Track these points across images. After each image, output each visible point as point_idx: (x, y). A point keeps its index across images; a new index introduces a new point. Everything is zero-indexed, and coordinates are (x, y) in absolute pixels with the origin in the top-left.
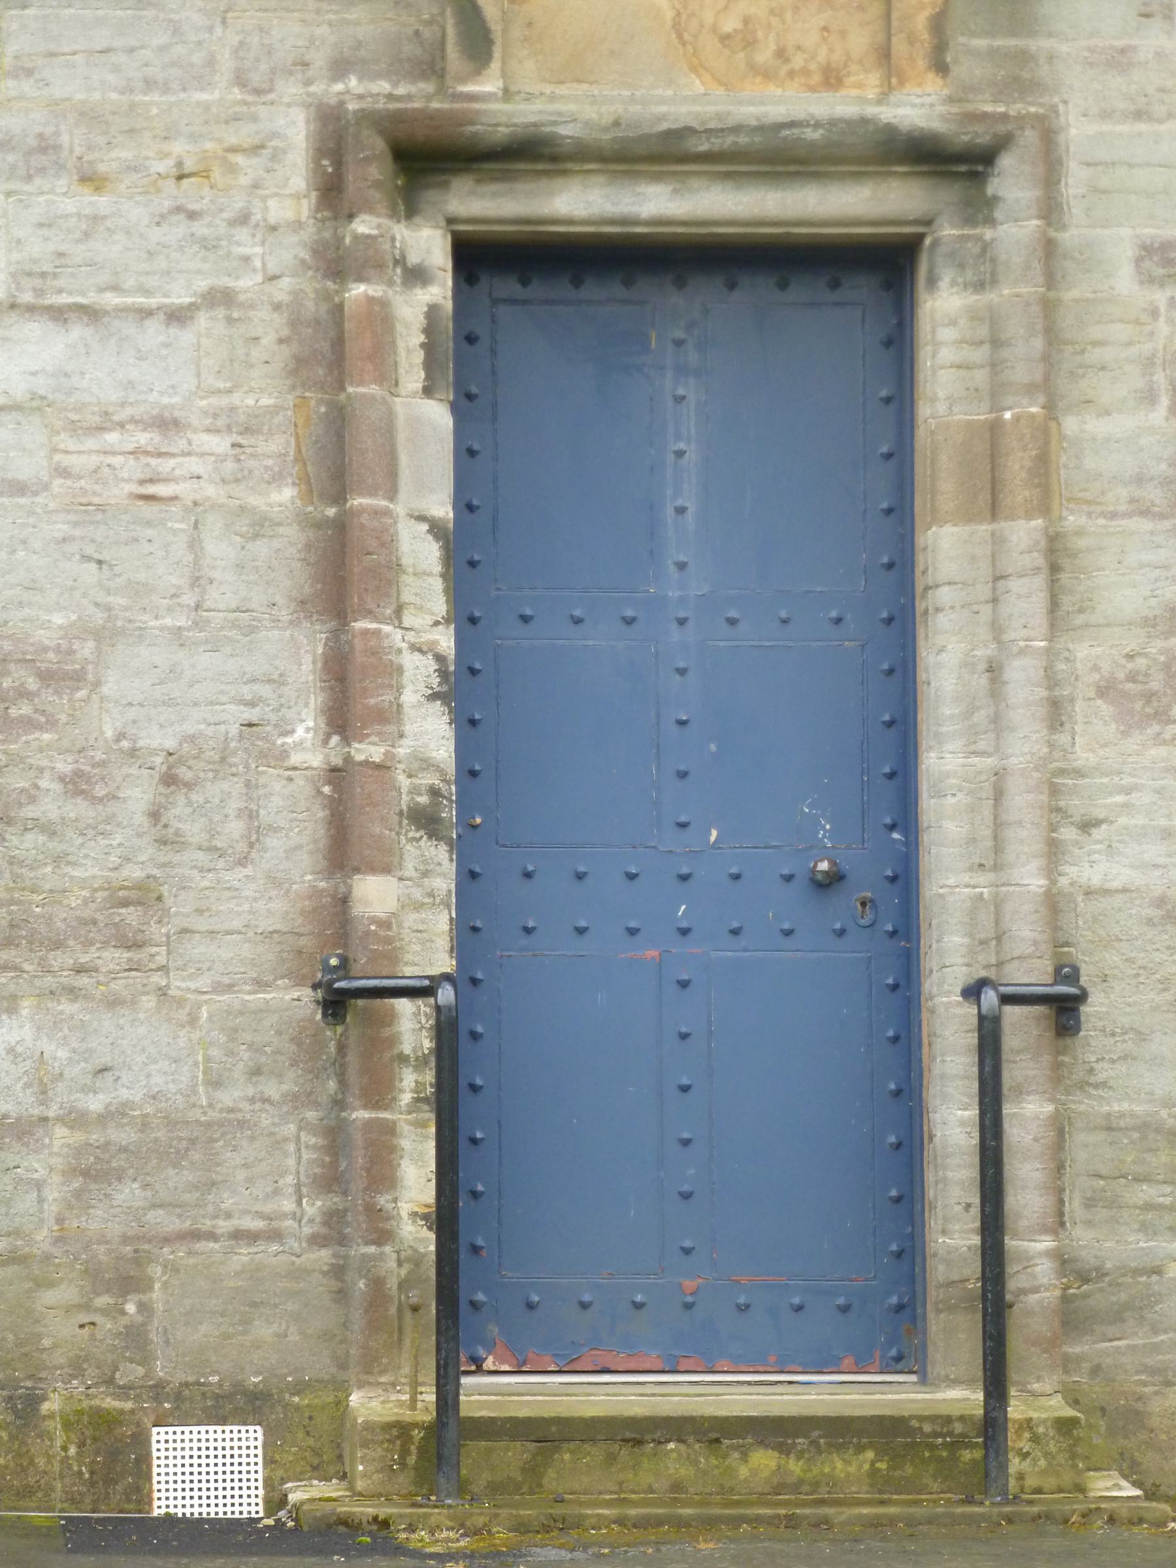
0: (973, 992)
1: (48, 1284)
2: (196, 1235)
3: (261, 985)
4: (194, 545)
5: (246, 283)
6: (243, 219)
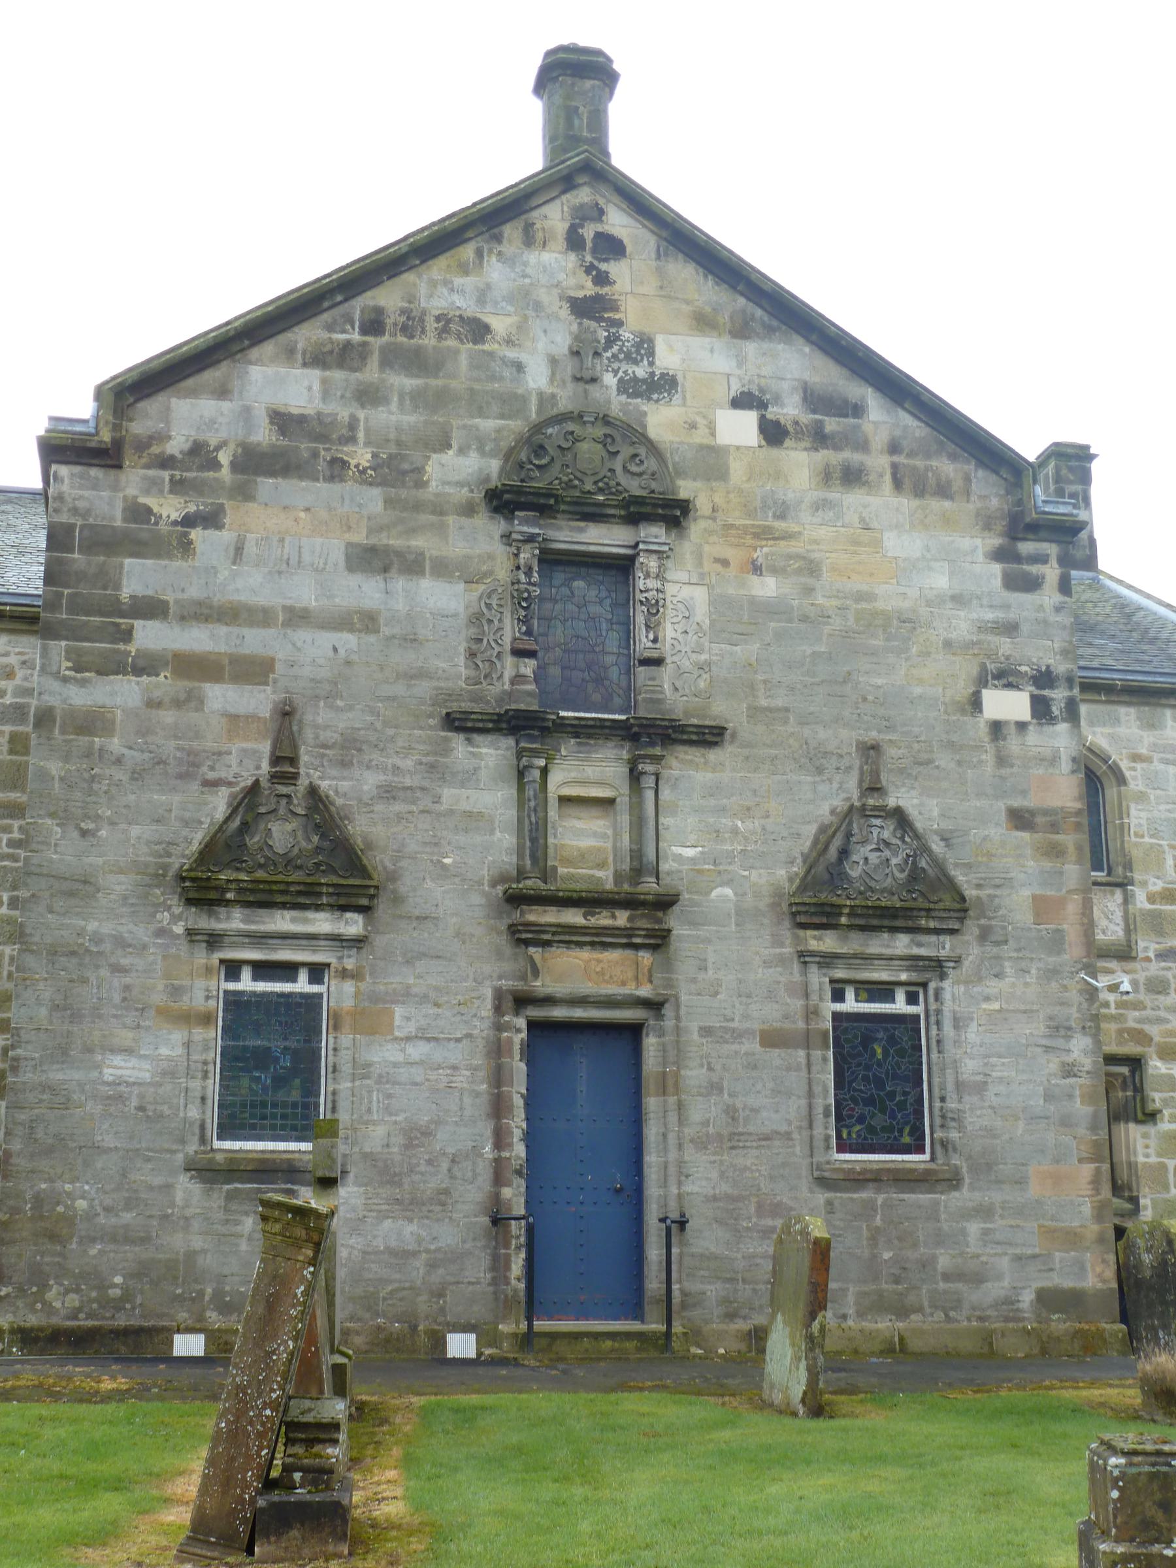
0: (663, 1220)
1: (418, 1295)
2: (458, 1283)
3: (476, 1216)
4: (461, 1099)
5: (476, 1032)
6: (475, 1016)
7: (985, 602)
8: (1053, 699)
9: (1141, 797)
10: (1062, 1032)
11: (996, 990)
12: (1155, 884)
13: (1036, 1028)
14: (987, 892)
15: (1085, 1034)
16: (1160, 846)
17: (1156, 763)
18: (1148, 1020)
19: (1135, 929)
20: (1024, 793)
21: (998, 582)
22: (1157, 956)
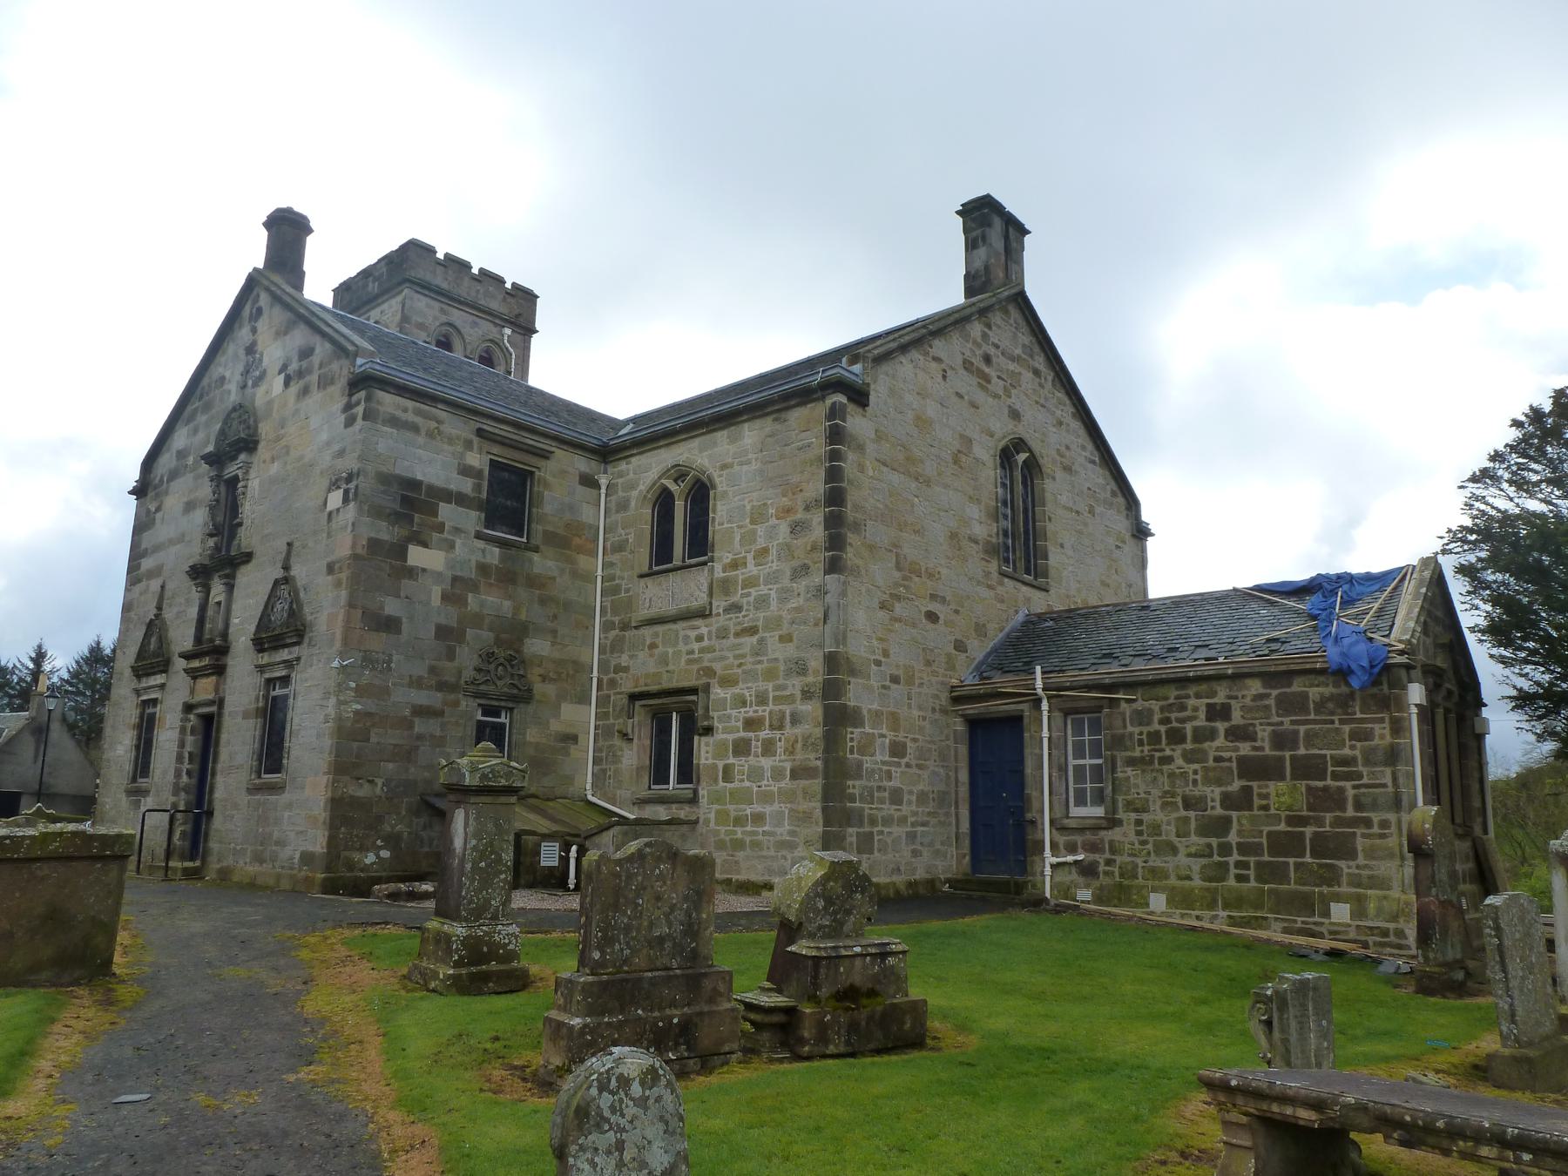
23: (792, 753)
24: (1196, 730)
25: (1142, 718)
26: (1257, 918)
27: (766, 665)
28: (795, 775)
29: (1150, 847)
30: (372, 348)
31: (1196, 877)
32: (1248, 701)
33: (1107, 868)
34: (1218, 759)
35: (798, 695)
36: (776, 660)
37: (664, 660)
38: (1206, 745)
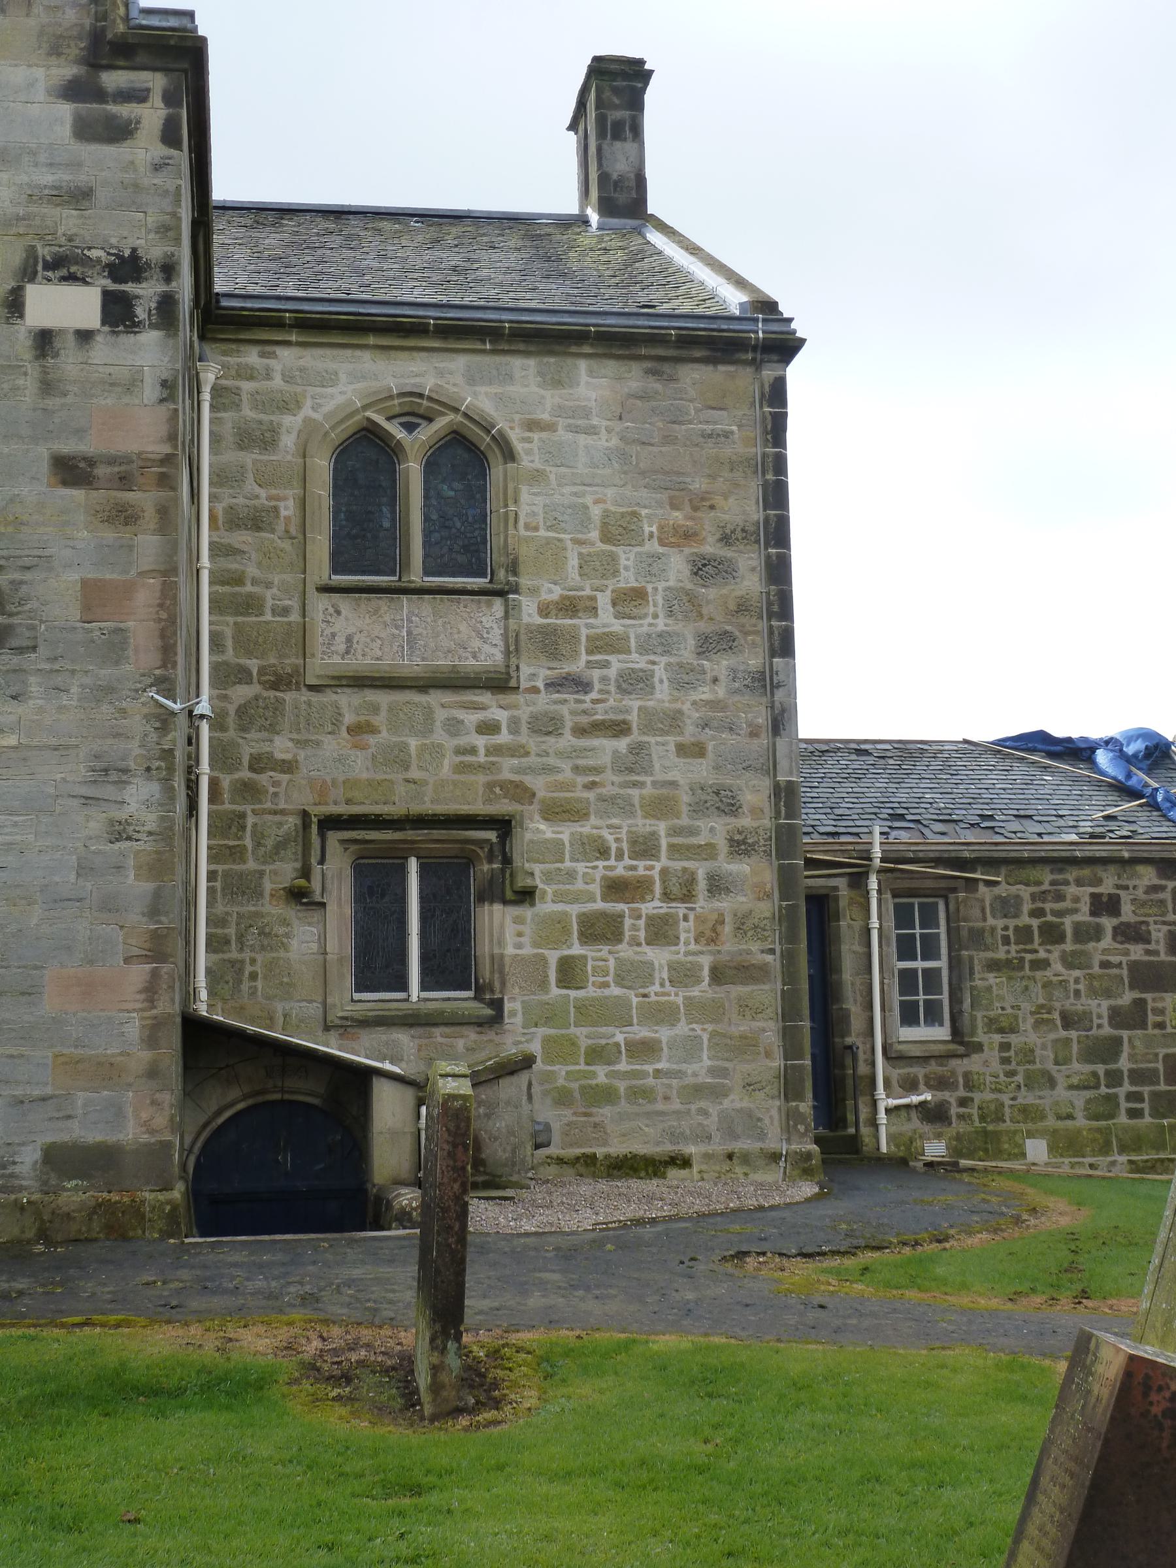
7: (42, 158)
8: (138, 297)
9: (537, 477)
10: (114, 776)
11: (13, 718)
12: (550, 591)
13: (75, 772)
14: (10, 577)
15: (149, 779)
16: (560, 540)
17: (561, 431)
18: (530, 770)
19: (517, 650)
20: (80, 432)
21: (65, 130)
22: (547, 685)
23: (713, 941)
24: (1077, 927)
25: (1007, 907)
26: (1162, 1161)
27: (648, 791)
28: (718, 975)
29: (1019, 1078)
30: (593, 89)
31: (1079, 1114)
32: (1140, 893)
33: (962, 1110)
34: (1105, 965)
35: (723, 847)
36: (673, 784)
37: (398, 758)
38: (1091, 945)
